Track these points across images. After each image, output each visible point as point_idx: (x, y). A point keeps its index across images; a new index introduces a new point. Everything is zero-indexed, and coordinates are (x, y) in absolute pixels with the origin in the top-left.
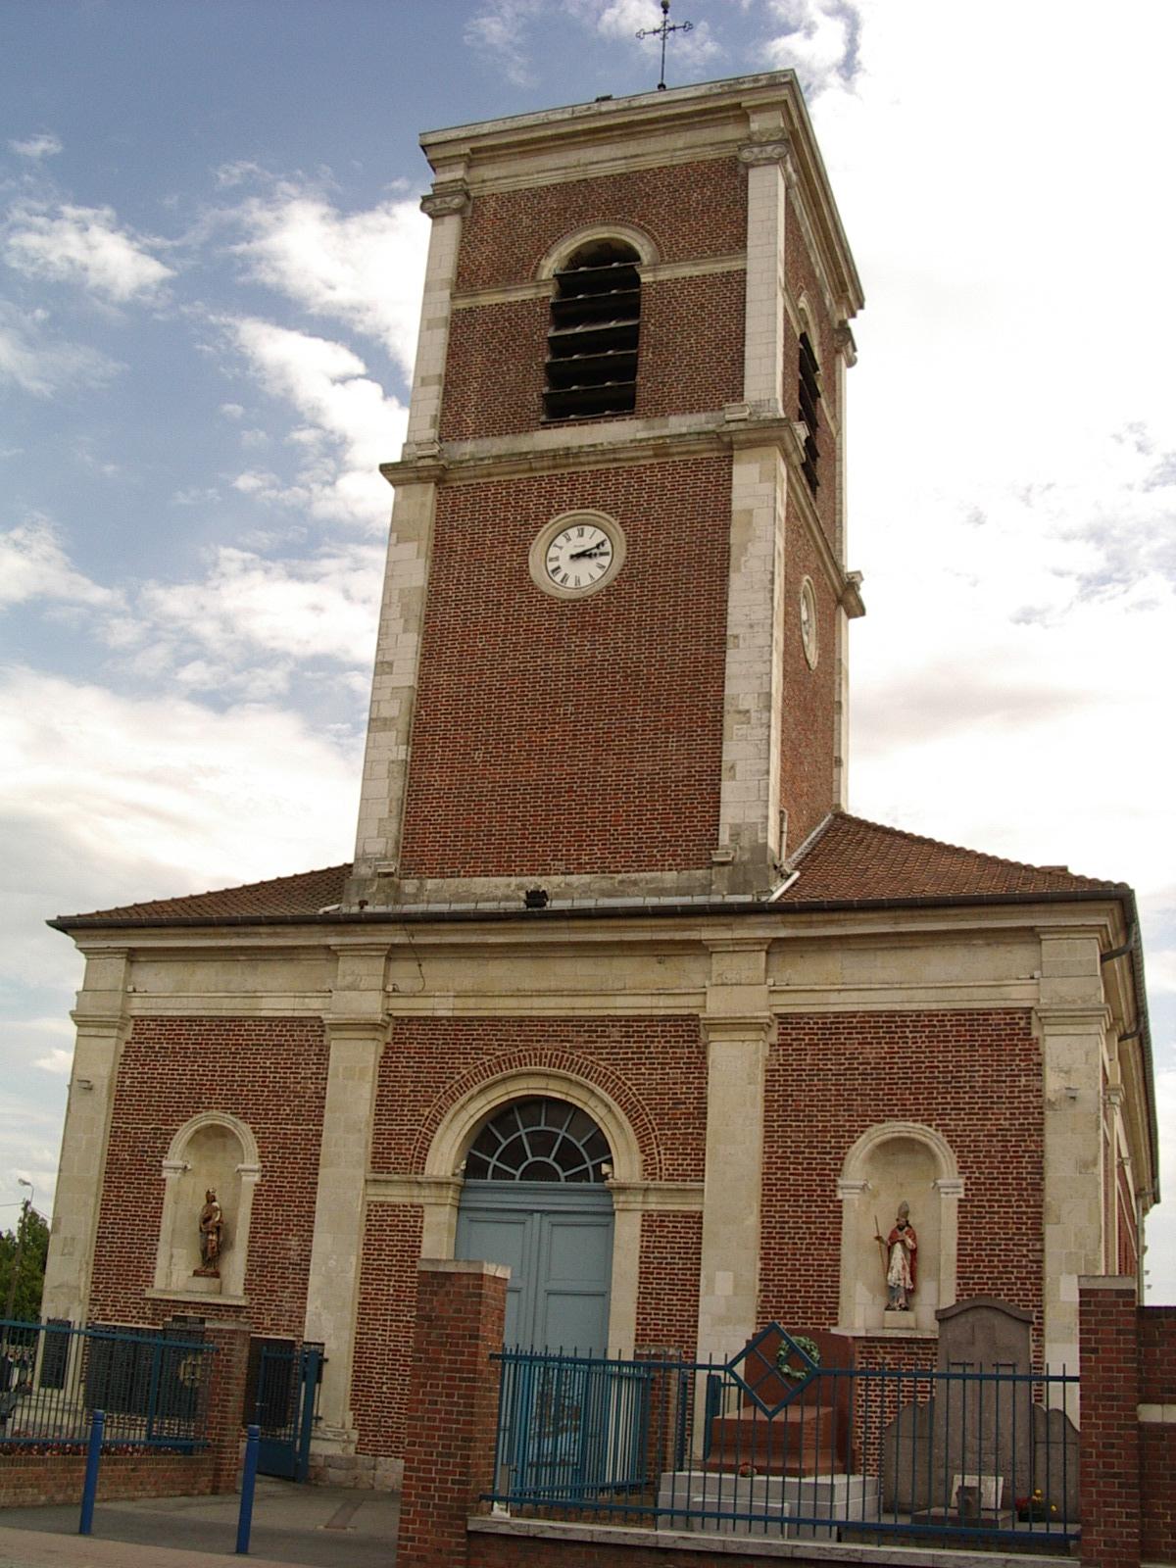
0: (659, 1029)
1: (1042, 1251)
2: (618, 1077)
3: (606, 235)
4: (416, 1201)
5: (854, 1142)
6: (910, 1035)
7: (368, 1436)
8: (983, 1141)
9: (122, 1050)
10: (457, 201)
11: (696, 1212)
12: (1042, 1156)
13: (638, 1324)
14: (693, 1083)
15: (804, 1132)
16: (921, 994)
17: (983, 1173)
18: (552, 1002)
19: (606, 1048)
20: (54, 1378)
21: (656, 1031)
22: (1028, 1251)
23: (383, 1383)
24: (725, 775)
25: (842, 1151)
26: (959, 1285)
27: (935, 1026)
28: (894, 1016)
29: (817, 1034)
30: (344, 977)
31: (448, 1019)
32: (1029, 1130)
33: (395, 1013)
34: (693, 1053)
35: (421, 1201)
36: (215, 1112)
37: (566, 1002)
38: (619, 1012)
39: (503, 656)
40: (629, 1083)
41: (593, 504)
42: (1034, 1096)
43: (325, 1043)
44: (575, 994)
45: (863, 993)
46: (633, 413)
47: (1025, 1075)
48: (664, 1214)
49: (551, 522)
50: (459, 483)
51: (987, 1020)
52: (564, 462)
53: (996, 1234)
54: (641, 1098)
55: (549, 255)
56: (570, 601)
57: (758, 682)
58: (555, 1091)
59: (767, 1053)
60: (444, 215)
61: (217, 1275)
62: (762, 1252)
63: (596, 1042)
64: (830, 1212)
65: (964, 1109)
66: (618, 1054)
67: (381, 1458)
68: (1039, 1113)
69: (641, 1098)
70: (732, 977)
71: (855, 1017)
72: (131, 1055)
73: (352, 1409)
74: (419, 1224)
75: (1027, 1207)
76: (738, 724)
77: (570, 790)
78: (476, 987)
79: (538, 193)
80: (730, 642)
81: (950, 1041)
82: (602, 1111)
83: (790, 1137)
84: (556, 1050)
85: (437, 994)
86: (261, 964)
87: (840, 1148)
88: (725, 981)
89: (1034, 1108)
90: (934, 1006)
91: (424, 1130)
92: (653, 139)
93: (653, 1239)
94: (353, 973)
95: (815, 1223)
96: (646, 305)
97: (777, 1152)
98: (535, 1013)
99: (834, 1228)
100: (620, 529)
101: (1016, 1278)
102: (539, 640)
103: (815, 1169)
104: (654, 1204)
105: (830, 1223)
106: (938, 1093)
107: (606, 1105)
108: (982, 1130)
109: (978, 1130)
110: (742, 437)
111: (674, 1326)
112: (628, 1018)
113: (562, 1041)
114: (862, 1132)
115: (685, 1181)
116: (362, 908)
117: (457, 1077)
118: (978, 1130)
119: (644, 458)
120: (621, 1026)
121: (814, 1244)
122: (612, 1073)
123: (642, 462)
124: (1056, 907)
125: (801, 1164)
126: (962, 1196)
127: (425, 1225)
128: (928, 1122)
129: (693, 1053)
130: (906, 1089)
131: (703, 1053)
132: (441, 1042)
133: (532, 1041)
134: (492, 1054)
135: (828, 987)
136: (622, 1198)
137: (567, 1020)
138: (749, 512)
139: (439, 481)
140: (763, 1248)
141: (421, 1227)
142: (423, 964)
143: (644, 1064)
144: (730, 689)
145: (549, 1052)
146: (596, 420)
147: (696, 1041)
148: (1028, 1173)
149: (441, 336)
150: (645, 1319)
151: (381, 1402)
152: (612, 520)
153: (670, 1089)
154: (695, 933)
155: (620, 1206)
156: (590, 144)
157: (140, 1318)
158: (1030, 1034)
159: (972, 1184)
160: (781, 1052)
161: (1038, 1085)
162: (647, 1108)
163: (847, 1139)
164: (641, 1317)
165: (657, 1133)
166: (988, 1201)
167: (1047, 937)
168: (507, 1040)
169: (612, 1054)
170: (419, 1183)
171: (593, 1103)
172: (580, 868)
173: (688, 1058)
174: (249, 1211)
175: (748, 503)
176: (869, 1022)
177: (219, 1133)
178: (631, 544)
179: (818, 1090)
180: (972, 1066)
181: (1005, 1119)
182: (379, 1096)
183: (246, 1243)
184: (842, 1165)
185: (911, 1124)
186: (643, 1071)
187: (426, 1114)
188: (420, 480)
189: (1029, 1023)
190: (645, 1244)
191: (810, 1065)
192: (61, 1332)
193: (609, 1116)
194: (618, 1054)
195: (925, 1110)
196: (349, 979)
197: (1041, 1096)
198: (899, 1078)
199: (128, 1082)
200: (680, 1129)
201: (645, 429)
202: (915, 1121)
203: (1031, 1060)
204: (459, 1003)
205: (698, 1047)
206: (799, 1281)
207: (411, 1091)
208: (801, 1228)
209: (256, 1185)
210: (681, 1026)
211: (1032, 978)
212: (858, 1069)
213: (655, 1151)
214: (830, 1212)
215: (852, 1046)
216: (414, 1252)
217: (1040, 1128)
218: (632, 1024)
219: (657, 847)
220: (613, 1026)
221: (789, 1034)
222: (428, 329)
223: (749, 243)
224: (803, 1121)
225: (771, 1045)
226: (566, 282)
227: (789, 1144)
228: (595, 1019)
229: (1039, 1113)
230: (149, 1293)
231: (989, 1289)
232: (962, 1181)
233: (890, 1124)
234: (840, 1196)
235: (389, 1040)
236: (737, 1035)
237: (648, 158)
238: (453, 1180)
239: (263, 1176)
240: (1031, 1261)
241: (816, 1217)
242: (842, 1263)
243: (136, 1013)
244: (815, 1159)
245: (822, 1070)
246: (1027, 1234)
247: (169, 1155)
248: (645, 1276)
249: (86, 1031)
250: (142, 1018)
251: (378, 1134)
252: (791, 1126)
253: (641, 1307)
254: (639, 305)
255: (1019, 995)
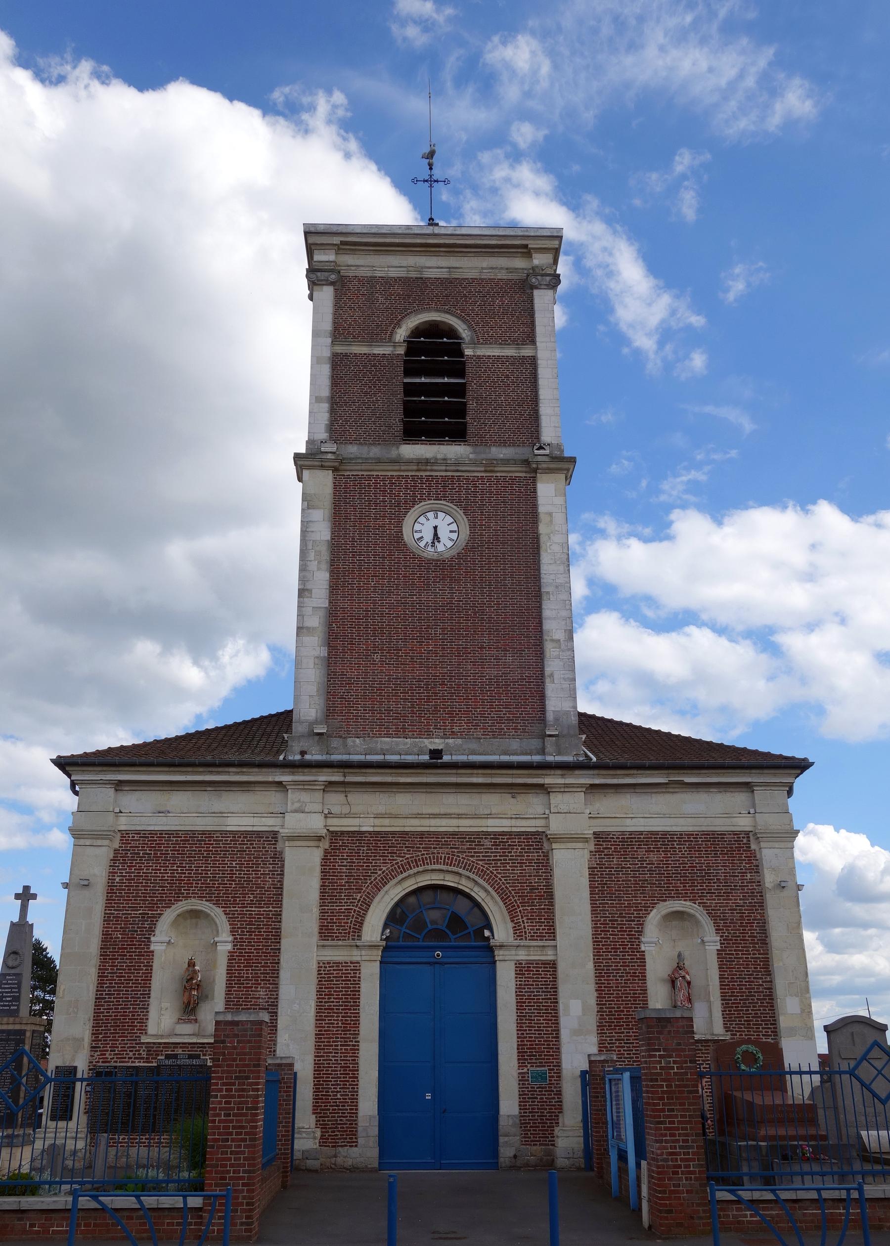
0: (517, 840)
1: (771, 982)
2: (491, 872)
3: (439, 319)
4: (355, 959)
5: (649, 914)
6: (677, 847)
7: (328, 1132)
8: (728, 913)
9: (111, 856)
10: (333, 277)
11: (551, 961)
12: (765, 923)
13: (518, 1038)
14: (542, 876)
15: (616, 907)
16: (682, 821)
17: (730, 933)
18: (444, 822)
19: (482, 852)
20: (63, 1112)
21: (515, 842)
22: (763, 982)
23: (337, 1092)
24: (547, 680)
25: (641, 919)
26: (723, 1004)
27: (692, 841)
28: (666, 835)
29: (619, 845)
30: (293, 804)
31: (370, 833)
32: (755, 906)
33: (331, 829)
34: (540, 856)
35: (358, 959)
36: (193, 900)
37: (455, 822)
38: (490, 830)
39: (389, 592)
40: (499, 876)
41: (444, 498)
42: (756, 886)
43: (278, 849)
44: (459, 816)
45: (647, 820)
46: (466, 441)
47: (750, 873)
48: (529, 962)
49: (416, 507)
50: (348, 473)
51: (724, 838)
52: (424, 468)
53: (742, 971)
54: (508, 885)
55: (400, 327)
56: (433, 560)
57: (564, 623)
58: (450, 881)
59: (589, 857)
60: (323, 285)
61: (196, 1021)
62: (597, 986)
63: (475, 849)
64: (637, 959)
65: (715, 893)
66: (491, 856)
67: (340, 1149)
68: (760, 896)
69: (508, 885)
70: (564, 808)
71: (642, 834)
72: (119, 859)
73: (314, 1113)
74: (357, 975)
75: (759, 954)
76: (553, 648)
77: (443, 684)
78: (388, 812)
79: (388, 282)
80: (544, 597)
81: (702, 851)
82: (483, 894)
83: (608, 910)
84: (447, 854)
85: (362, 816)
86: (224, 793)
87: (640, 917)
88: (560, 811)
89: (757, 893)
90: (691, 829)
91: (357, 909)
92: (466, 258)
93: (523, 979)
94: (299, 801)
95: (629, 966)
96: (469, 370)
97: (600, 920)
98: (432, 829)
99: (641, 969)
100: (464, 517)
101: (757, 999)
102: (413, 584)
103: (626, 931)
104: (522, 956)
105: (638, 966)
106: (698, 883)
107: (486, 890)
108: (728, 906)
109: (724, 906)
110: (544, 466)
111: (543, 1037)
112: (496, 834)
113: (451, 848)
114: (653, 907)
115: (543, 940)
116: (303, 756)
117: (380, 872)
118: (724, 906)
119: (477, 471)
120: (491, 838)
121: (629, 980)
122: (487, 869)
123: (476, 474)
124: (766, 771)
125: (617, 928)
126: (719, 948)
127: (362, 976)
128: (693, 901)
129: (540, 856)
130: (678, 880)
131: (547, 856)
132: (365, 848)
133: (431, 848)
134: (403, 857)
135: (625, 816)
136: (501, 952)
137: (454, 834)
138: (550, 514)
139: (335, 470)
140: (597, 983)
141: (359, 977)
142: (349, 795)
143: (509, 863)
144: (547, 625)
145: (443, 855)
146: (440, 443)
147: (541, 849)
148: (757, 933)
149: (326, 369)
150: (523, 1034)
151: (337, 1106)
152: (458, 509)
153: (527, 880)
154: (540, 779)
155: (501, 958)
156: (423, 254)
157: (135, 1058)
158: (750, 847)
159: (724, 940)
160: (597, 856)
161: (758, 878)
162: (513, 892)
163: (644, 912)
164: (520, 1032)
165: (521, 908)
166: (735, 951)
167: (758, 788)
168: (413, 847)
169: (486, 856)
170: (357, 946)
171: (476, 889)
172: (453, 735)
173: (537, 859)
174: (225, 972)
175: (549, 509)
176: (651, 838)
177: (195, 914)
178: (472, 527)
179: (623, 881)
180: (717, 866)
181: (740, 900)
182: (322, 886)
183: (223, 995)
184: (642, 928)
185: (684, 903)
186: (508, 868)
187: (358, 898)
188: (322, 467)
189: (749, 841)
190: (518, 983)
191: (617, 864)
192: (68, 1074)
193: (489, 898)
194: (491, 856)
195: (691, 893)
196: (297, 805)
197: (760, 885)
198: (673, 873)
199: (117, 879)
200: (536, 906)
201: (474, 453)
202: (685, 900)
203: (752, 863)
204: (378, 822)
205: (542, 852)
206: (622, 1004)
207: (346, 882)
208: (620, 969)
209: (229, 952)
210: (531, 839)
211: (749, 813)
212: (646, 867)
213: (521, 920)
214: (637, 959)
215: (641, 853)
216: (355, 995)
217: (762, 904)
218: (497, 837)
219: (504, 723)
220: (485, 838)
221: (601, 845)
222: (318, 363)
223: (538, 339)
224: (615, 900)
225: (591, 852)
226: (412, 347)
227: (608, 915)
228: (472, 833)
229: (760, 896)
230: (144, 1039)
231: (741, 1007)
232: (719, 938)
233: (671, 902)
234: (643, 949)
235: (327, 847)
236: (570, 845)
237: (464, 271)
238: (381, 944)
239: (234, 945)
240: (765, 988)
241: (629, 962)
242: (648, 992)
243: (123, 828)
244: (625, 924)
245: (624, 868)
246: (761, 972)
247: (157, 932)
248: (520, 1004)
249: (82, 842)
250: (127, 832)
251: (323, 912)
252: (608, 903)
253: (520, 1025)
254: (465, 370)
255: (743, 823)
